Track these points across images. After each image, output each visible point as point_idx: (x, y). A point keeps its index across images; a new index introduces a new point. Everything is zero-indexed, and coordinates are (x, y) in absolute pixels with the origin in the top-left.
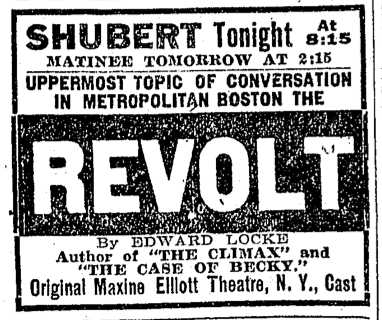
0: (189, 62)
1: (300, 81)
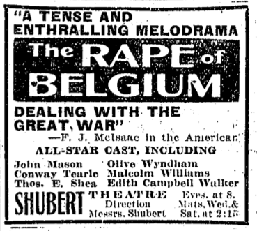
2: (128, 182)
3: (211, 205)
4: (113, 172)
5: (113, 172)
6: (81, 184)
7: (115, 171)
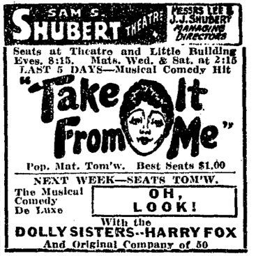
0: (185, 179)
1: (76, 232)
2: (118, 221)
3: (106, 223)
4: (60, 165)
5: (60, 165)
6: (26, 193)
7: (98, 58)
